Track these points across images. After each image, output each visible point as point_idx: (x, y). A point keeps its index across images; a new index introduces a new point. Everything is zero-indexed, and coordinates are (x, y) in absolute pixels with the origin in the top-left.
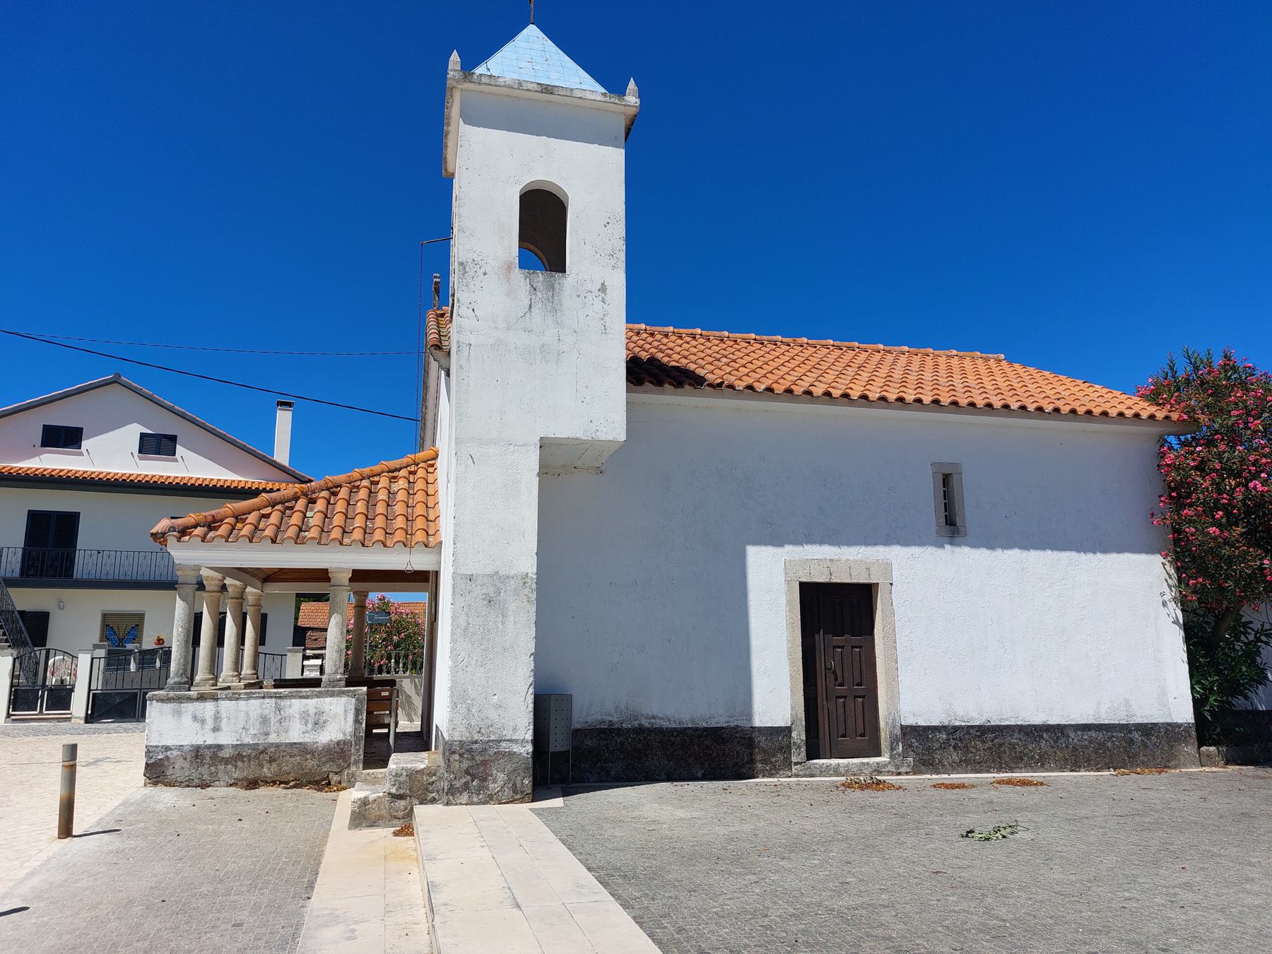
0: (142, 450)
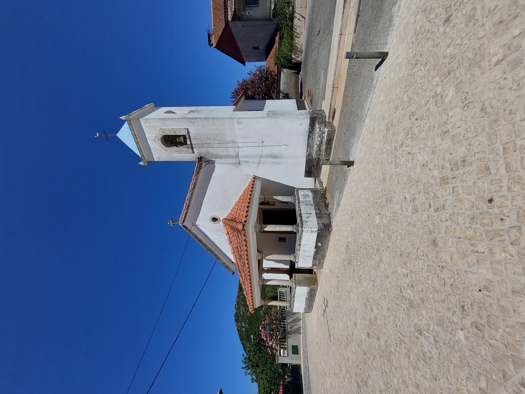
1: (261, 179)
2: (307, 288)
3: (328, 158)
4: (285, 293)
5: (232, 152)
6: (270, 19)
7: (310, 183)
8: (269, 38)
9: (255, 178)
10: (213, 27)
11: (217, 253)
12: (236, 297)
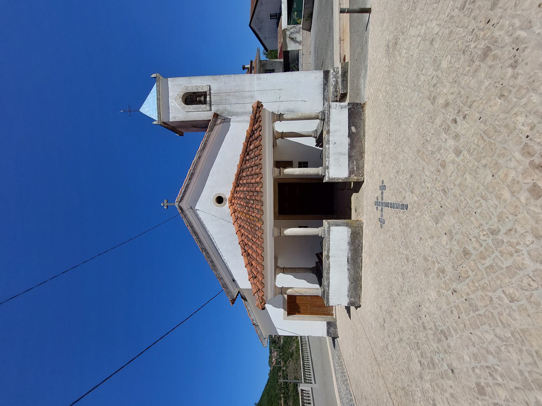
3: (345, 92)
4: (310, 392)
9: (271, 19)
11: (214, 259)
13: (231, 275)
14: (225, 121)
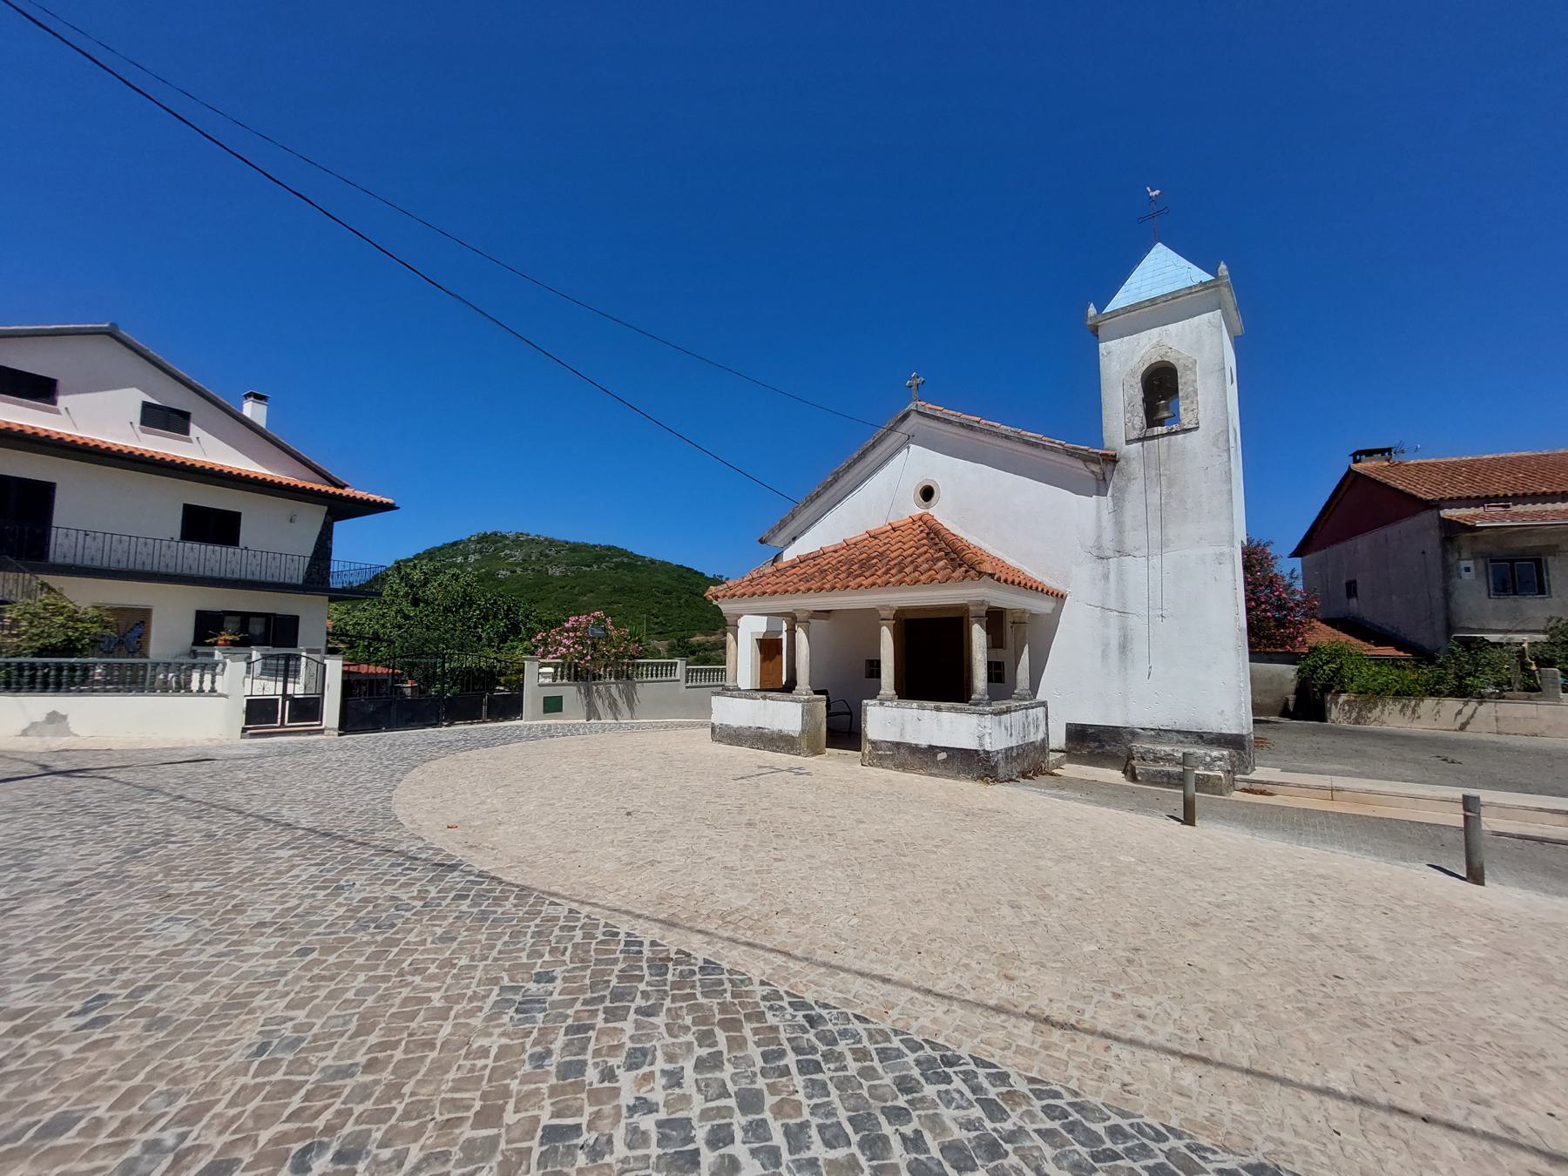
0: (144, 422)
1: (1057, 612)
2: (799, 728)
3: (1139, 778)
4: (673, 678)
5: (1134, 538)
6: (1450, 628)
7: (1058, 739)
8: (1388, 628)
9: (1060, 597)
10: (1412, 462)
11: (824, 498)
12: (549, 537)
13: (802, 533)
14: (1101, 483)
